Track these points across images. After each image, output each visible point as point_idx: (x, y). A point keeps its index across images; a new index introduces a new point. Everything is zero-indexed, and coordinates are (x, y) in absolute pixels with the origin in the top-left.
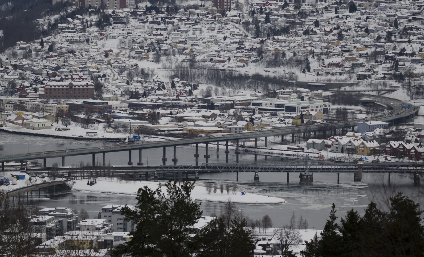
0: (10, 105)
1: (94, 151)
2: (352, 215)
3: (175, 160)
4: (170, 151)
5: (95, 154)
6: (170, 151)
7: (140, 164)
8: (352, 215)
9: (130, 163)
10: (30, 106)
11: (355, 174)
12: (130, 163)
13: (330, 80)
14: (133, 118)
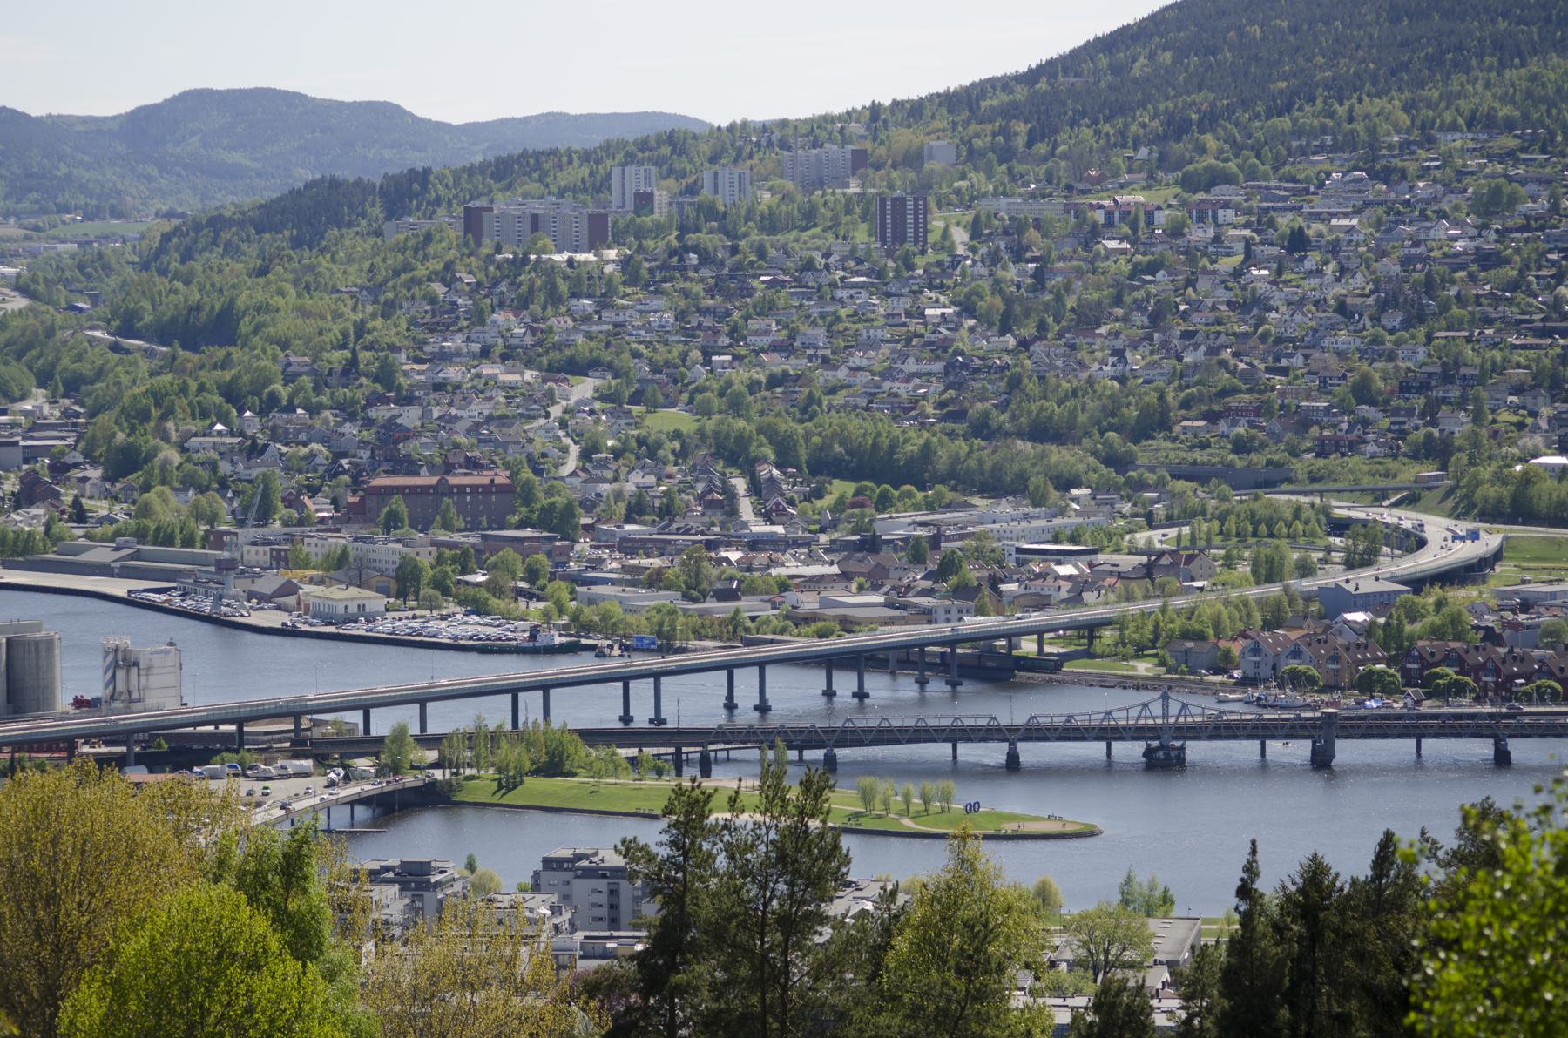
0: (260, 549)
1: (243, 713)
2: (1316, 874)
3: (763, 708)
4: (746, 681)
5: (521, 695)
6: (746, 681)
7: (658, 720)
8: (1316, 874)
9: (626, 718)
10: (319, 550)
11: (1314, 743)
12: (626, 718)
13: (1195, 463)
14: (633, 583)
